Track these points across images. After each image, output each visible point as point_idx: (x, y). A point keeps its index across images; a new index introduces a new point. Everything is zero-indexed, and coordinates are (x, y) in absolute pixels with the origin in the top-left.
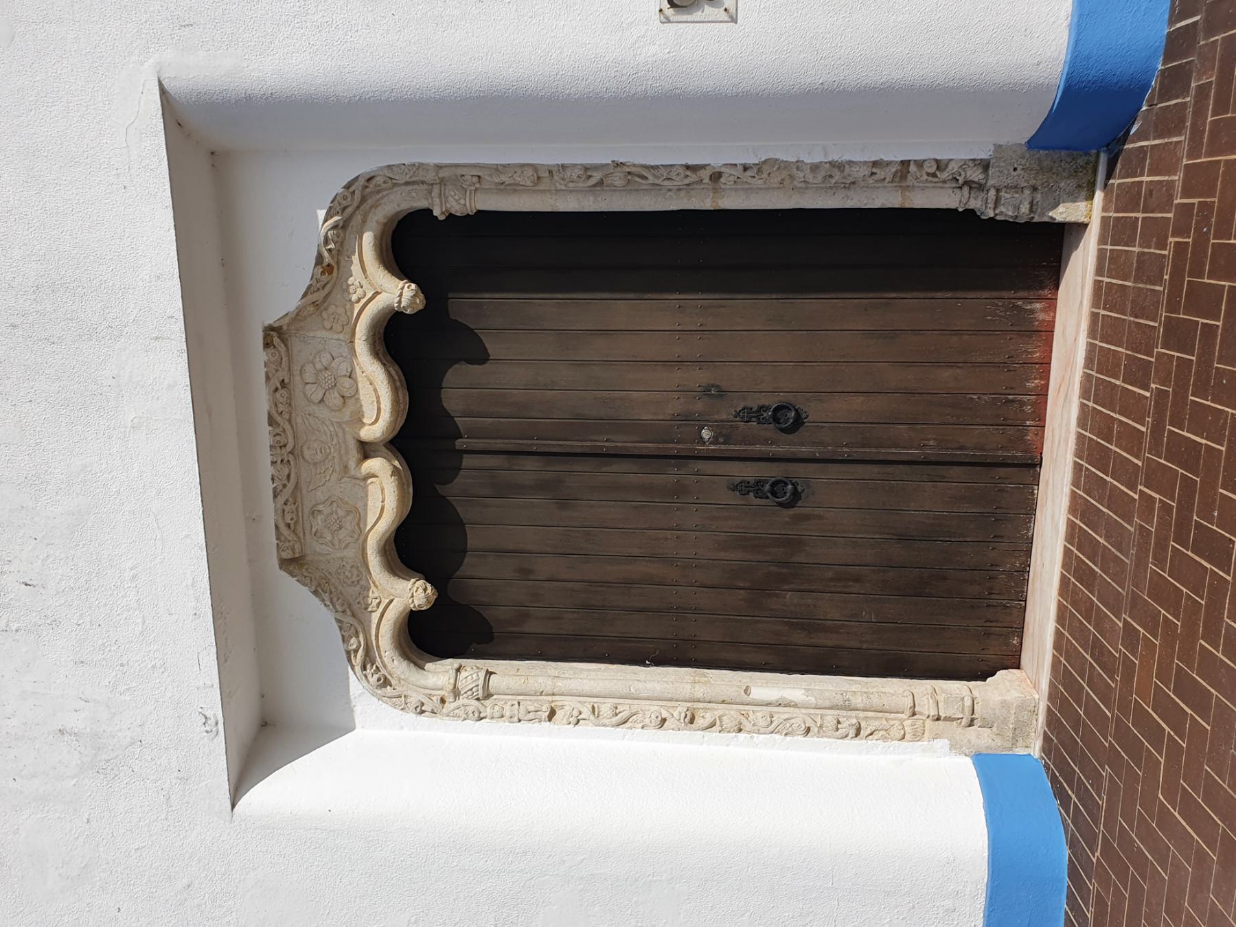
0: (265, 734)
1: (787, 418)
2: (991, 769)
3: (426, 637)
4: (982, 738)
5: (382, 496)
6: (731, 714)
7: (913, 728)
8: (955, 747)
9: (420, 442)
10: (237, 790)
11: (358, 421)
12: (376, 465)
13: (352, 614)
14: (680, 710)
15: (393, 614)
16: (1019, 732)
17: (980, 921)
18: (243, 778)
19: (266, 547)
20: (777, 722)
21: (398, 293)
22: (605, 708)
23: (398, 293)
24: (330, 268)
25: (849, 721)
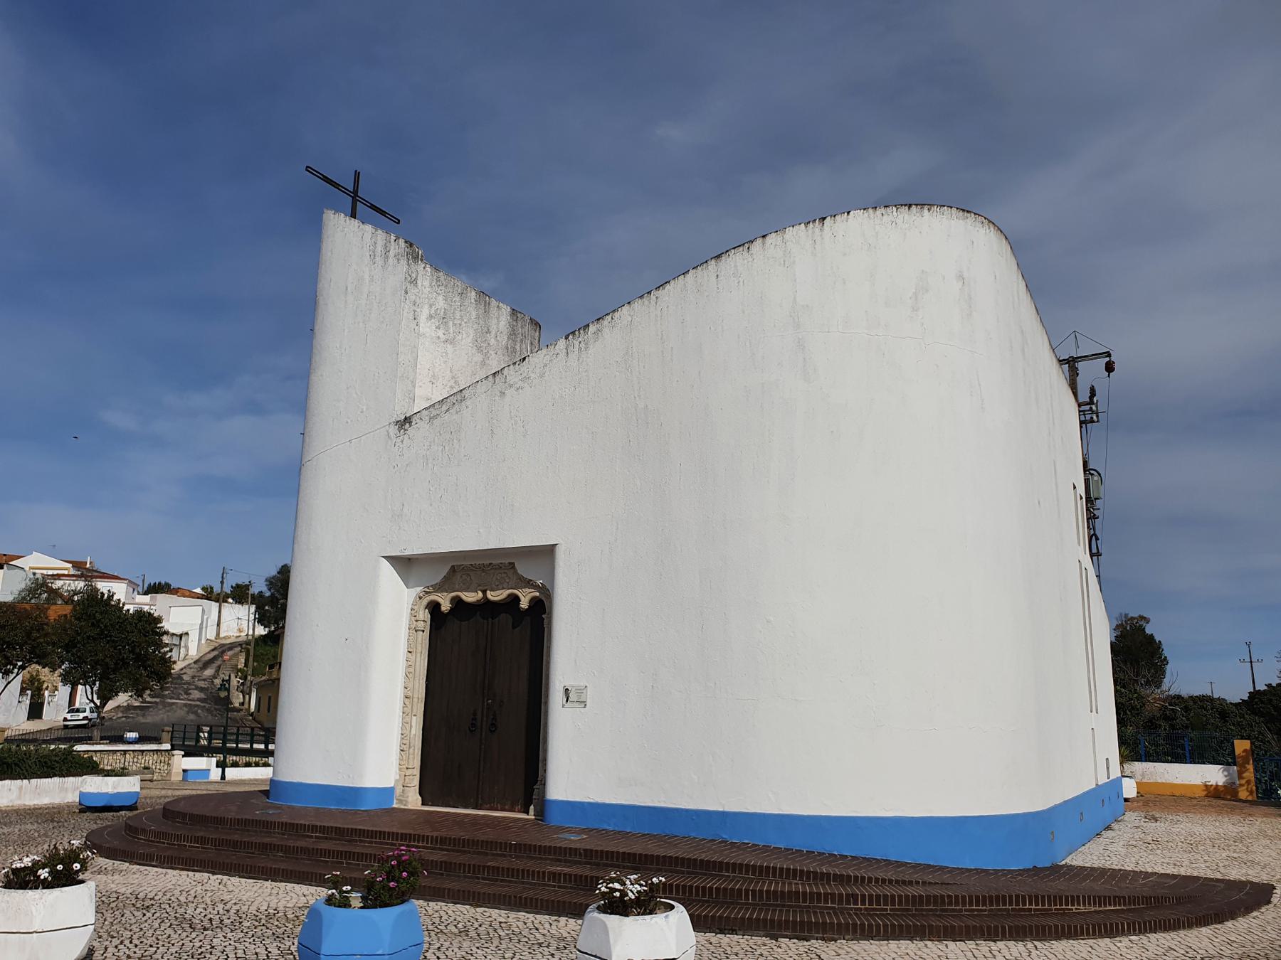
0: (404, 564)
1: (493, 727)
2: (389, 792)
3: (434, 608)
4: (399, 790)
5: (471, 597)
6: (408, 710)
7: (403, 768)
8: (397, 781)
9: (486, 606)
10: (392, 560)
11: (492, 590)
12: (480, 594)
13: (439, 588)
14: (410, 694)
15: (440, 600)
16: (400, 801)
17: (2, 600)
18: (392, 560)
19: (462, 567)
20: (405, 724)
21: (524, 604)
22: (411, 670)
23: (524, 604)
24: (529, 584)
25: (405, 748)
